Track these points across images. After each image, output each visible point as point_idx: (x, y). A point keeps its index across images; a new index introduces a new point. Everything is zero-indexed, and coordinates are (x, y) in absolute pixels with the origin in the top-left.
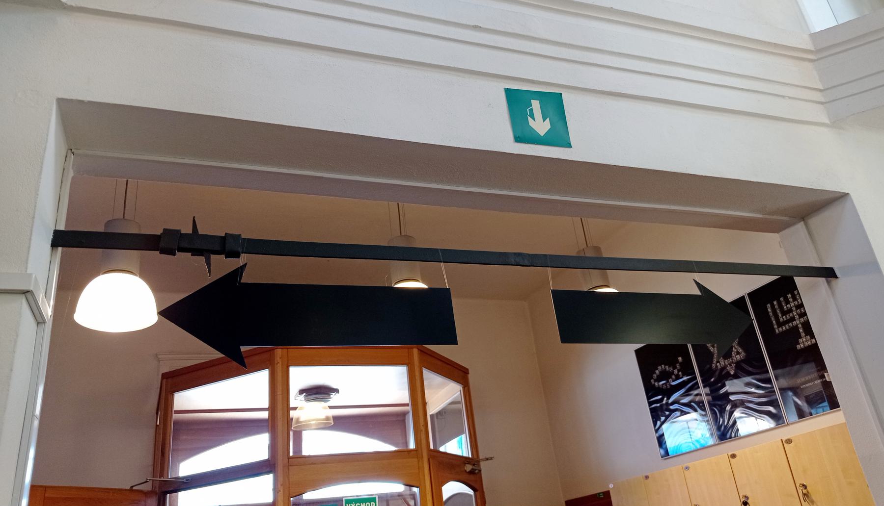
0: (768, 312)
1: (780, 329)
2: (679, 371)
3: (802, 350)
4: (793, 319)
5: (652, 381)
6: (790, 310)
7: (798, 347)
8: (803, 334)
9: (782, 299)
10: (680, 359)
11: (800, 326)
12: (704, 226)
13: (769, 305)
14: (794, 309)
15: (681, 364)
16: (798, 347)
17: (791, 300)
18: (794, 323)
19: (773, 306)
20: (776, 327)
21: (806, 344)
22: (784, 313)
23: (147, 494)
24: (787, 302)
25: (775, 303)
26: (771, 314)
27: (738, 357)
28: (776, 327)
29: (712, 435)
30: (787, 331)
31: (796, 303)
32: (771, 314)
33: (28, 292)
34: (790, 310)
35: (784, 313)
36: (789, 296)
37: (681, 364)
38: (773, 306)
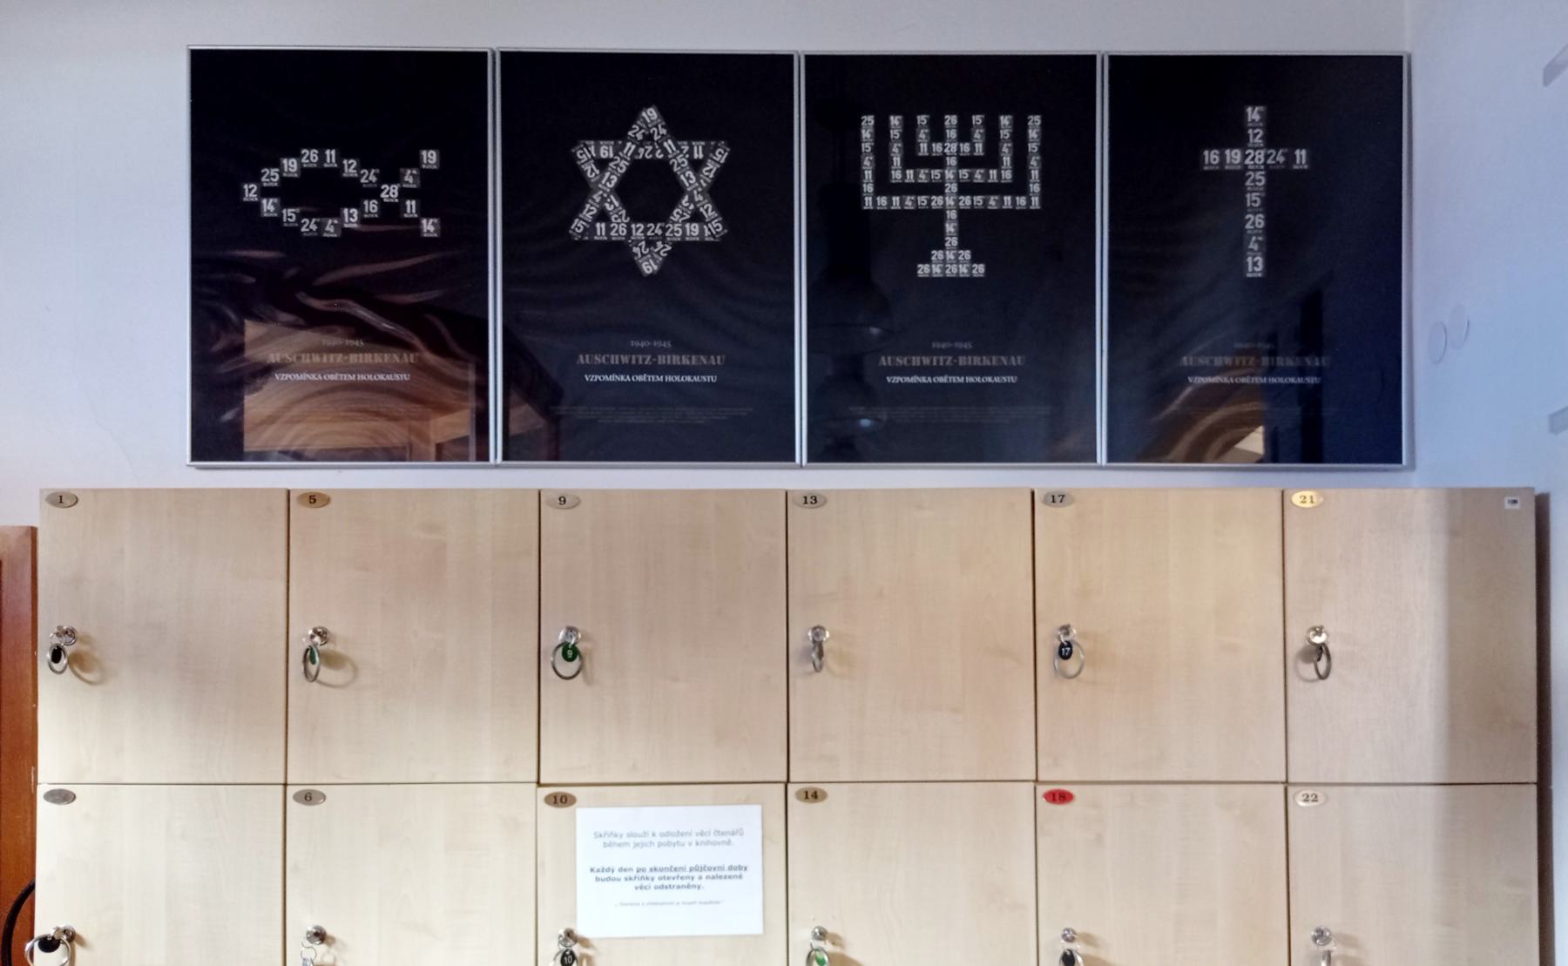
0: (858, 140)
1: (882, 201)
2: (405, 194)
3: (930, 281)
4: (937, 188)
5: (250, 192)
6: (938, 162)
7: (923, 270)
8: (952, 241)
9: (922, 119)
10: (430, 158)
11: (952, 215)
12: (958, 490)
13: (869, 121)
14: (952, 161)
15: (426, 175)
16: (923, 270)
17: (964, 173)
18: (937, 201)
19: (882, 131)
20: (869, 188)
21: (952, 271)
22: (912, 160)
23: (1295, 784)
24: (938, 134)
25: (895, 121)
26: (867, 147)
27: (693, 230)
28: (869, 188)
29: (256, 390)
30: (903, 213)
31: (966, 148)
32: (867, 147)
33: (821, 654)
34: (938, 162)
35: (912, 160)
36: (951, 120)
37: (426, 175)
38: (882, 131)
